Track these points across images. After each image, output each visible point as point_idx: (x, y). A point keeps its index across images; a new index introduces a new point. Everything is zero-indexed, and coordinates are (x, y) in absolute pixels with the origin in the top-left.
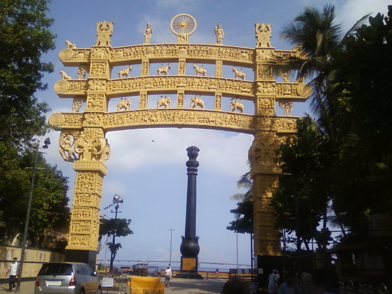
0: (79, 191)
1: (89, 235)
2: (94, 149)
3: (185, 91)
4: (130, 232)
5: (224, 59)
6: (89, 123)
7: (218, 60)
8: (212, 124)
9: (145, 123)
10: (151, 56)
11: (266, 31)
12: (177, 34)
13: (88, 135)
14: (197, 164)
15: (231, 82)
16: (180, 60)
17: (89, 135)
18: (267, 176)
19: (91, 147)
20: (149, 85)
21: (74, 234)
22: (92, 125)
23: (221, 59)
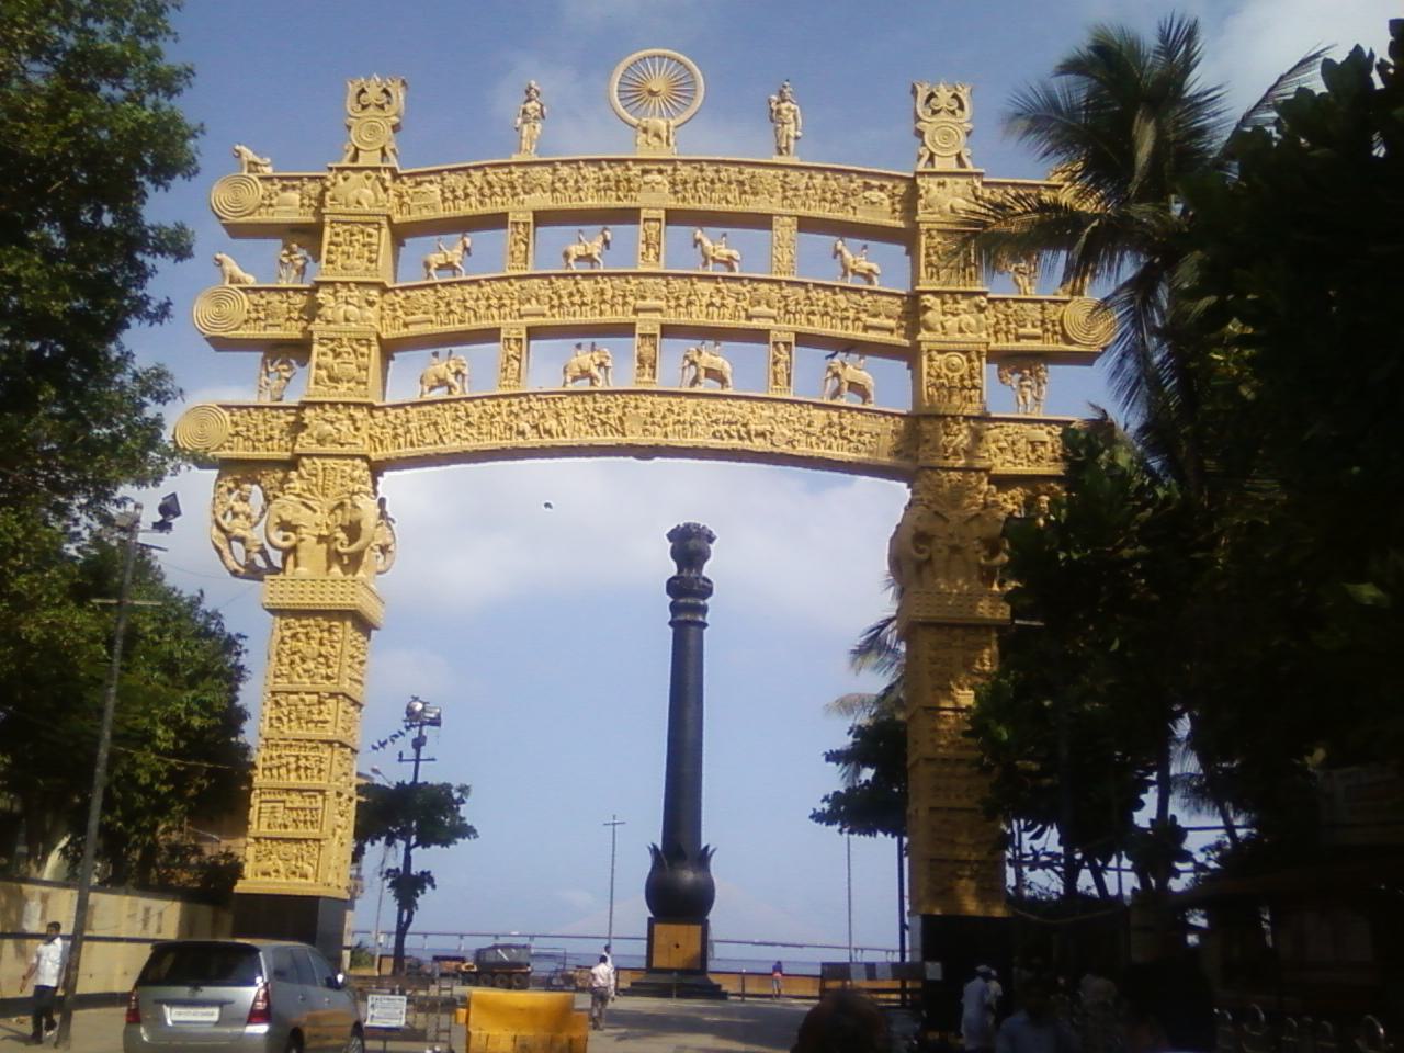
0: (283, 683)
1: (319, 840)
2: (337, 535)
3: (664, 327)
4: (466, 831)
5: (802, 211)
6: (320, 441)
7: (781, 215)
8: (759, 445)
9: (519, 442)
10: (542, 201)
11: (953, 112)
12: (635, 121)
13: (316, 485)
14: (704, 586)
15: (828, 293)
16: (644, 214)
17: (320, 483)
18: (958, 632)
19: (327, 526)
20: (533, 306)
21: (266, 839)
22: (329, 448)
23: (793, 212)
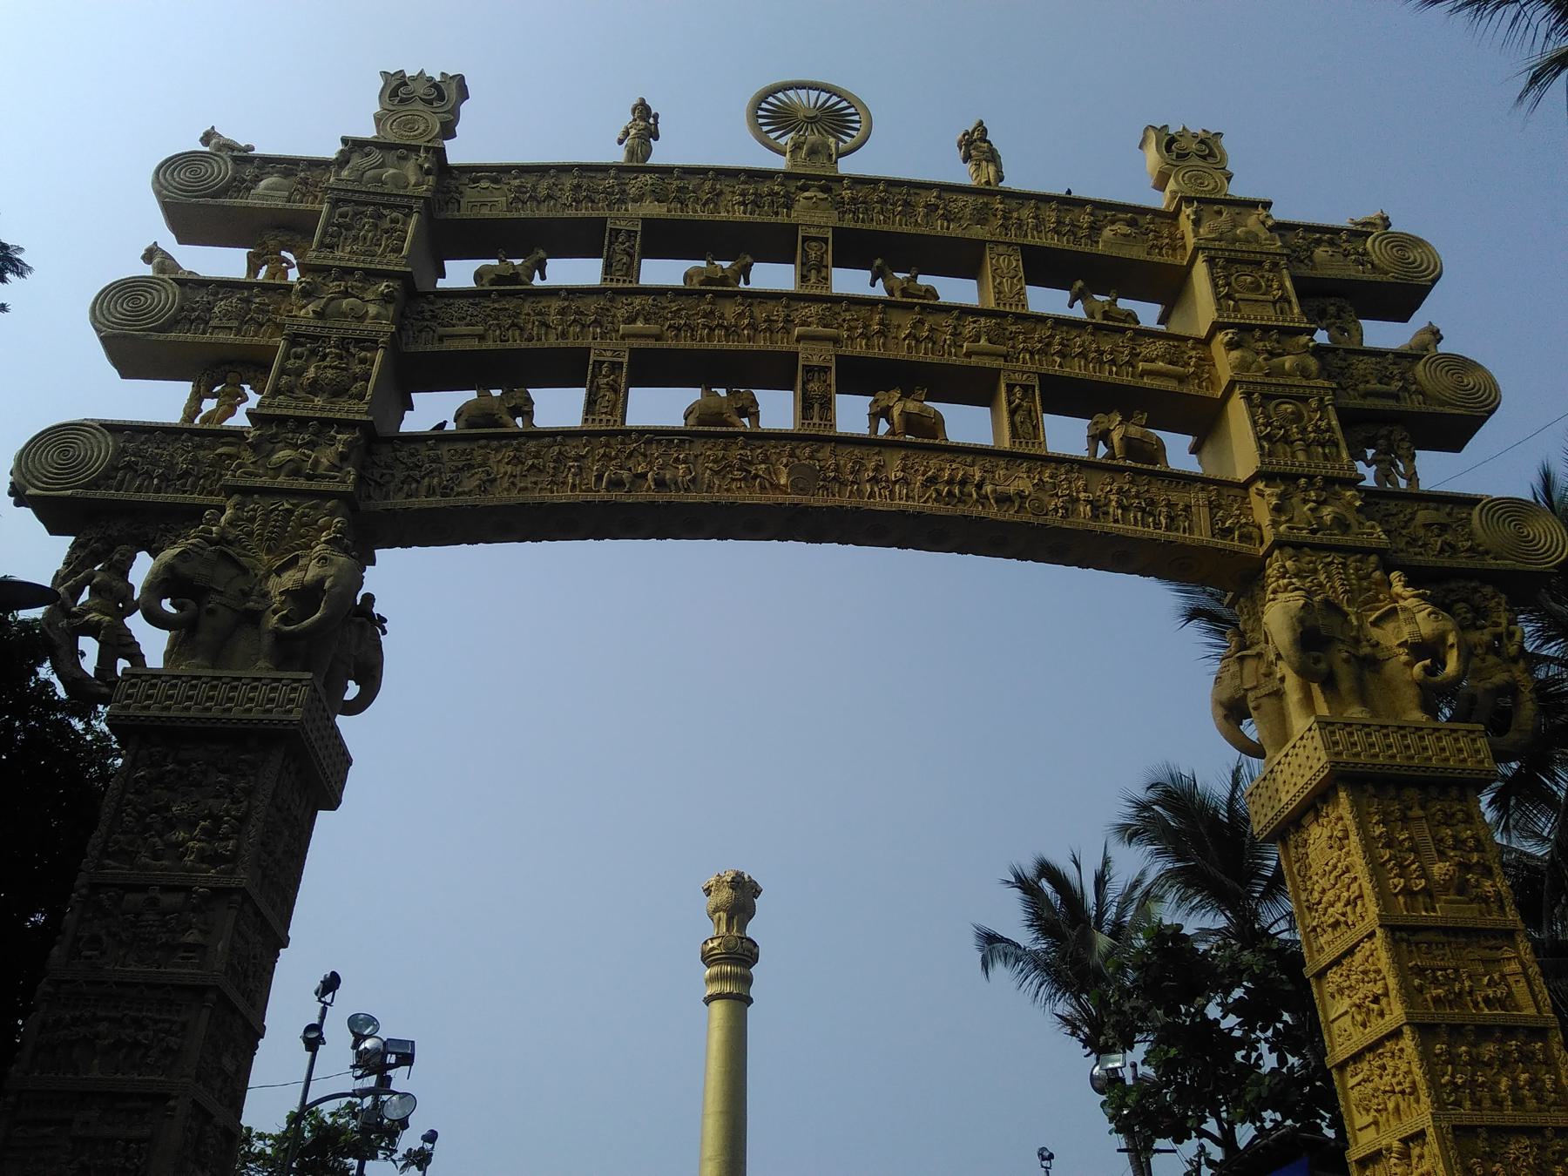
5: (1029, 240)
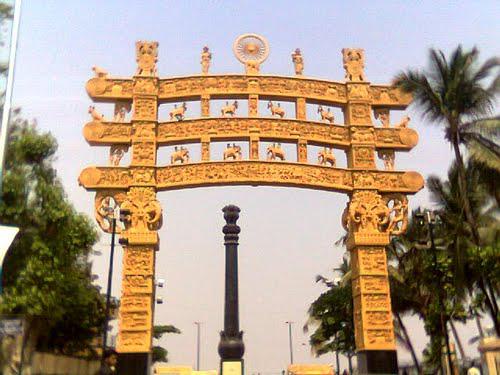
0: (130, 273)
6: (138, 181)
8: (298, 181)
9: (211, 181)
10: (215, 91)
12: (243, 60)
16: (250, 96)
20: (212, 130)
22: (141, 184)
